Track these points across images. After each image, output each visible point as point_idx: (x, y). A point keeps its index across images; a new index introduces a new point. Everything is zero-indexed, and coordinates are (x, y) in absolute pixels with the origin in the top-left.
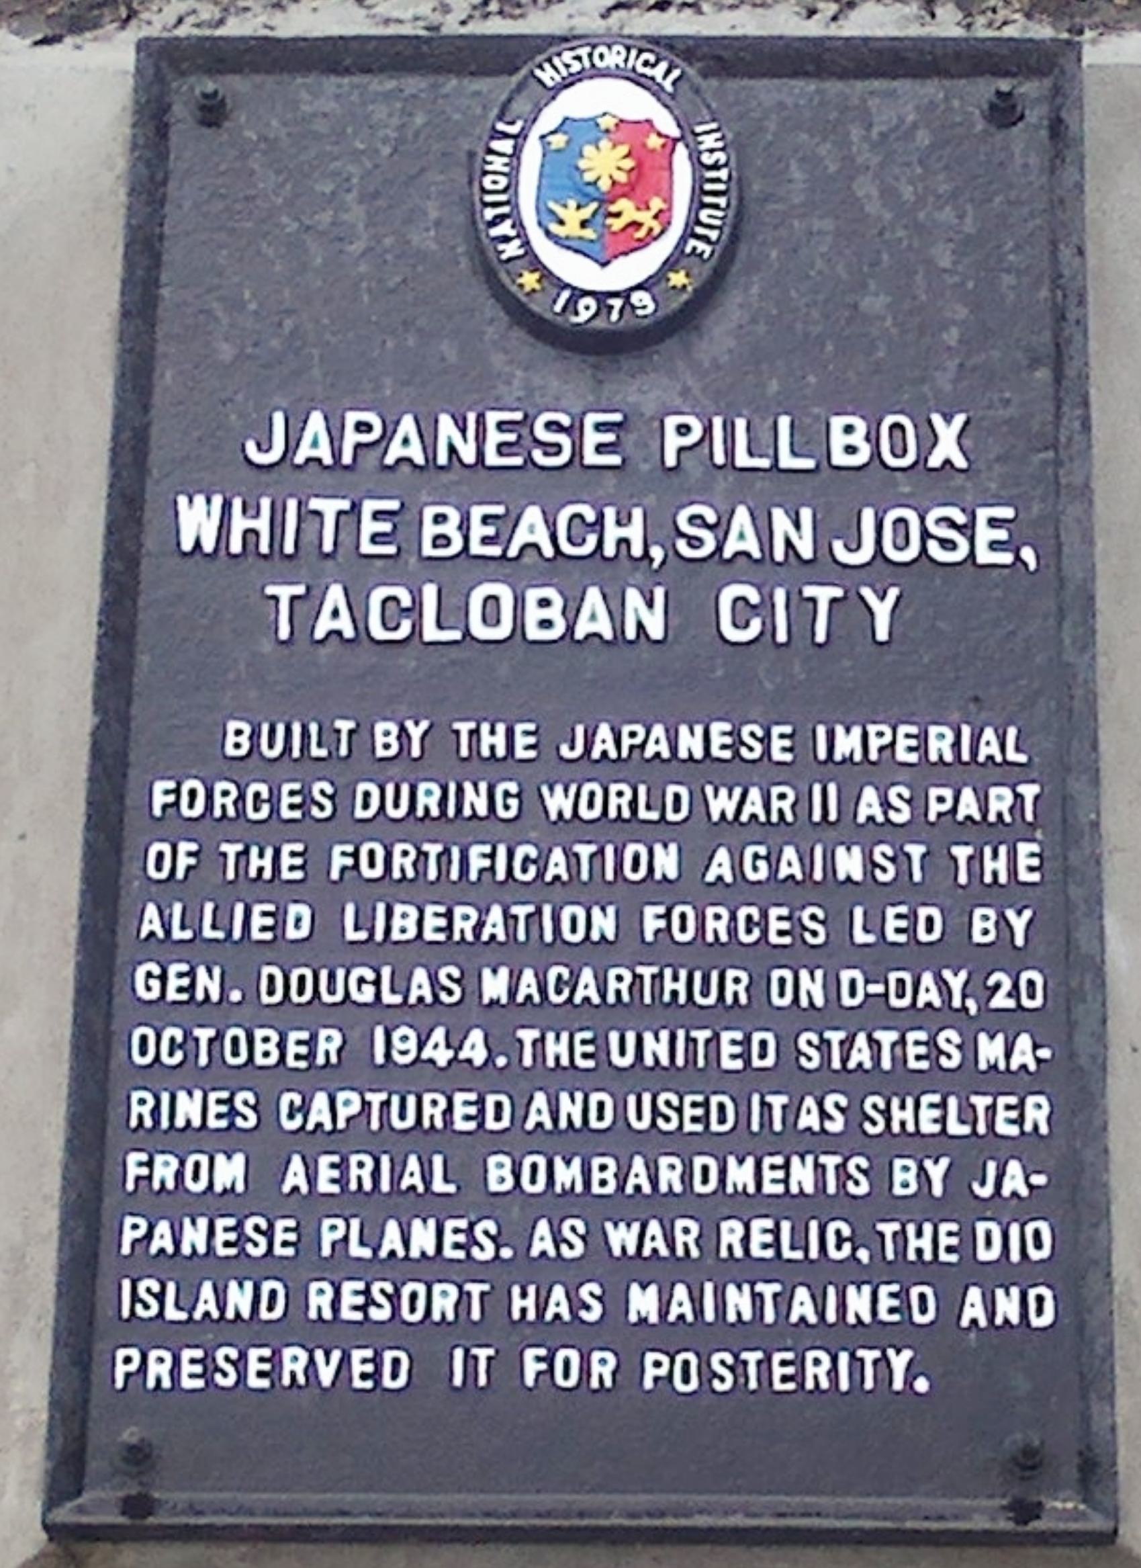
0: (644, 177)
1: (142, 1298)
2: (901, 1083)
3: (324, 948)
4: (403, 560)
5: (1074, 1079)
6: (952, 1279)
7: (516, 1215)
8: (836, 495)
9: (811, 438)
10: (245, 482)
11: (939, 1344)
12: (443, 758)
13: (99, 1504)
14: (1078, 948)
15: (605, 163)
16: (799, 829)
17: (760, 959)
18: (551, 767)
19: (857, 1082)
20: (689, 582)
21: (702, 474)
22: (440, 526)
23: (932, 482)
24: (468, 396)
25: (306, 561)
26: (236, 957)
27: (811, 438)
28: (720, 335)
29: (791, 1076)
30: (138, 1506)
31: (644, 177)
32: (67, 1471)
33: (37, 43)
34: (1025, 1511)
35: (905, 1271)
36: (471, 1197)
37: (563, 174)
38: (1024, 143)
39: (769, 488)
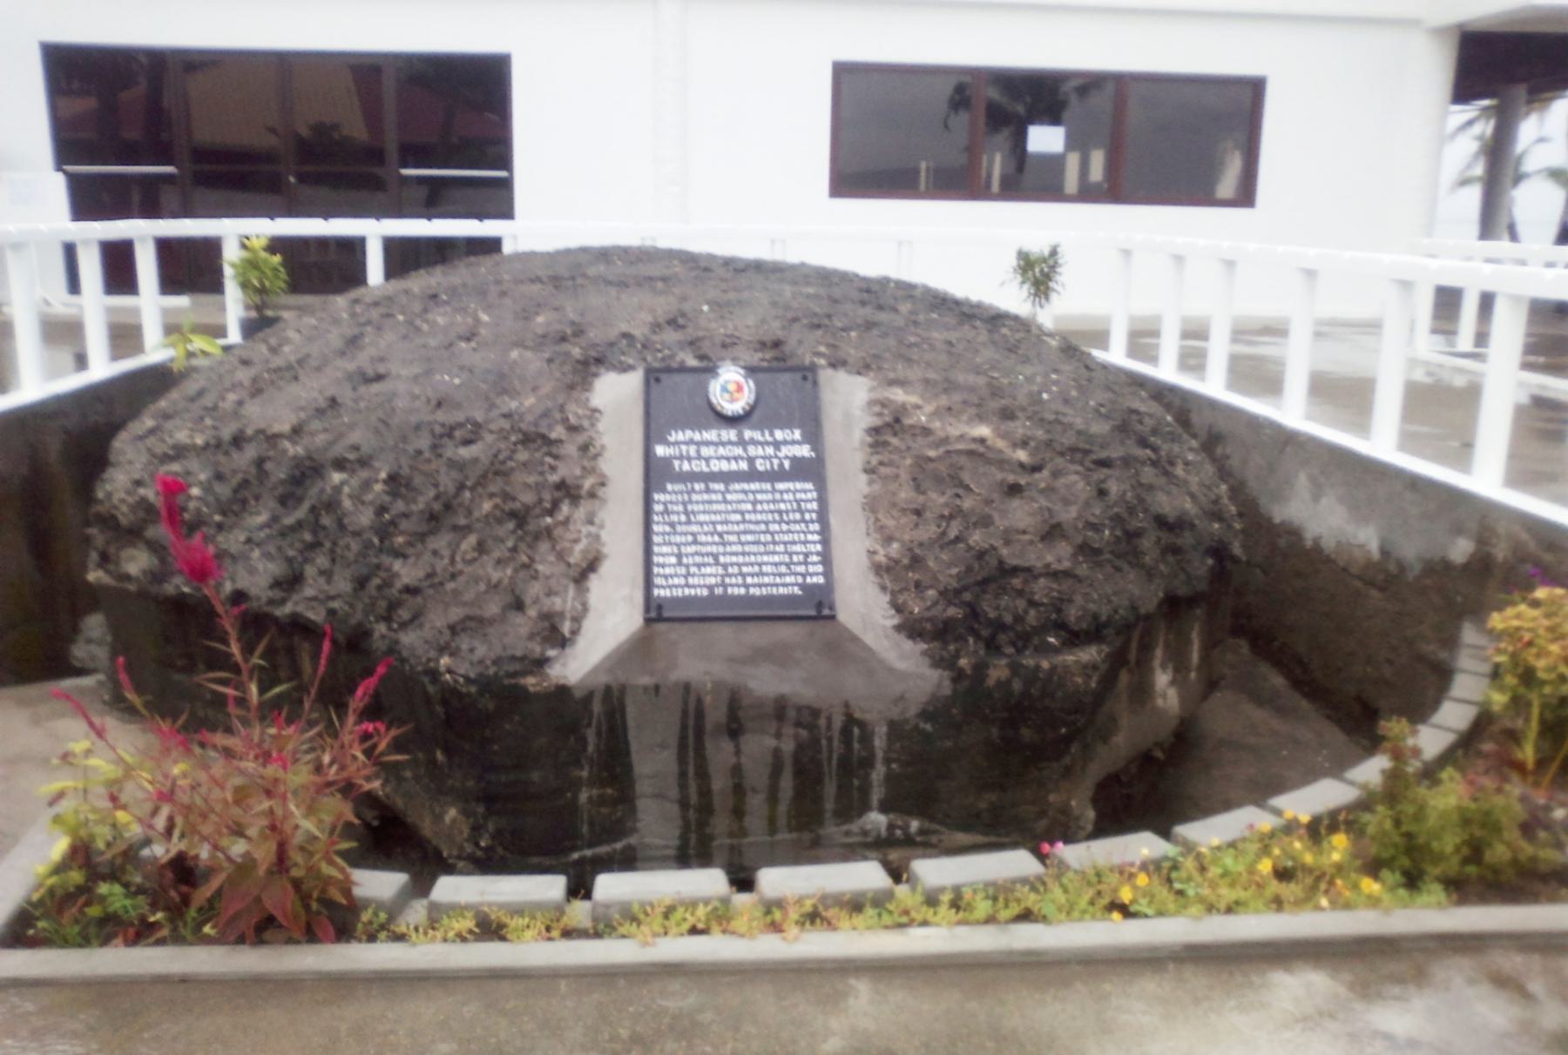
0: (740, 389)
1: (658, 581)
2: (794, 543)
3: (689, 522)
4: (699, 457)
5: (825, 542)
6: (804, 576)
7: (725, 566)
8: (777, 445)
9: (772, 434)
10: (668, 444)
11: (803, 586)
12: (708, 491)
13: (653, 614)
14: (564, 665)
15: (732, 387)
16: (774, 501)
17: (767, 523)
18: (728, 491)
19: (785, 543)
20: (751, 460)
21: (753, 442)
22: (705, 451)
23: (794, 442)
24: (707, 427)
25: (681, 458)
26: (672, 525)
27: (772, 434)
28: (755, 417)
29: (774, 543)
30: (659, 614)
31: (740, 389)
32: (647, 609)
33: (379, 378)
34: (819, 611)
35: (796, 574)
36: (717, 563)
37: (724, 389)
38: (809, 385)
39: (764, 444)
